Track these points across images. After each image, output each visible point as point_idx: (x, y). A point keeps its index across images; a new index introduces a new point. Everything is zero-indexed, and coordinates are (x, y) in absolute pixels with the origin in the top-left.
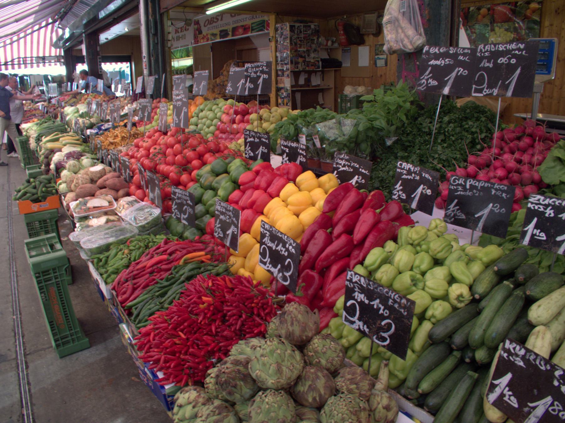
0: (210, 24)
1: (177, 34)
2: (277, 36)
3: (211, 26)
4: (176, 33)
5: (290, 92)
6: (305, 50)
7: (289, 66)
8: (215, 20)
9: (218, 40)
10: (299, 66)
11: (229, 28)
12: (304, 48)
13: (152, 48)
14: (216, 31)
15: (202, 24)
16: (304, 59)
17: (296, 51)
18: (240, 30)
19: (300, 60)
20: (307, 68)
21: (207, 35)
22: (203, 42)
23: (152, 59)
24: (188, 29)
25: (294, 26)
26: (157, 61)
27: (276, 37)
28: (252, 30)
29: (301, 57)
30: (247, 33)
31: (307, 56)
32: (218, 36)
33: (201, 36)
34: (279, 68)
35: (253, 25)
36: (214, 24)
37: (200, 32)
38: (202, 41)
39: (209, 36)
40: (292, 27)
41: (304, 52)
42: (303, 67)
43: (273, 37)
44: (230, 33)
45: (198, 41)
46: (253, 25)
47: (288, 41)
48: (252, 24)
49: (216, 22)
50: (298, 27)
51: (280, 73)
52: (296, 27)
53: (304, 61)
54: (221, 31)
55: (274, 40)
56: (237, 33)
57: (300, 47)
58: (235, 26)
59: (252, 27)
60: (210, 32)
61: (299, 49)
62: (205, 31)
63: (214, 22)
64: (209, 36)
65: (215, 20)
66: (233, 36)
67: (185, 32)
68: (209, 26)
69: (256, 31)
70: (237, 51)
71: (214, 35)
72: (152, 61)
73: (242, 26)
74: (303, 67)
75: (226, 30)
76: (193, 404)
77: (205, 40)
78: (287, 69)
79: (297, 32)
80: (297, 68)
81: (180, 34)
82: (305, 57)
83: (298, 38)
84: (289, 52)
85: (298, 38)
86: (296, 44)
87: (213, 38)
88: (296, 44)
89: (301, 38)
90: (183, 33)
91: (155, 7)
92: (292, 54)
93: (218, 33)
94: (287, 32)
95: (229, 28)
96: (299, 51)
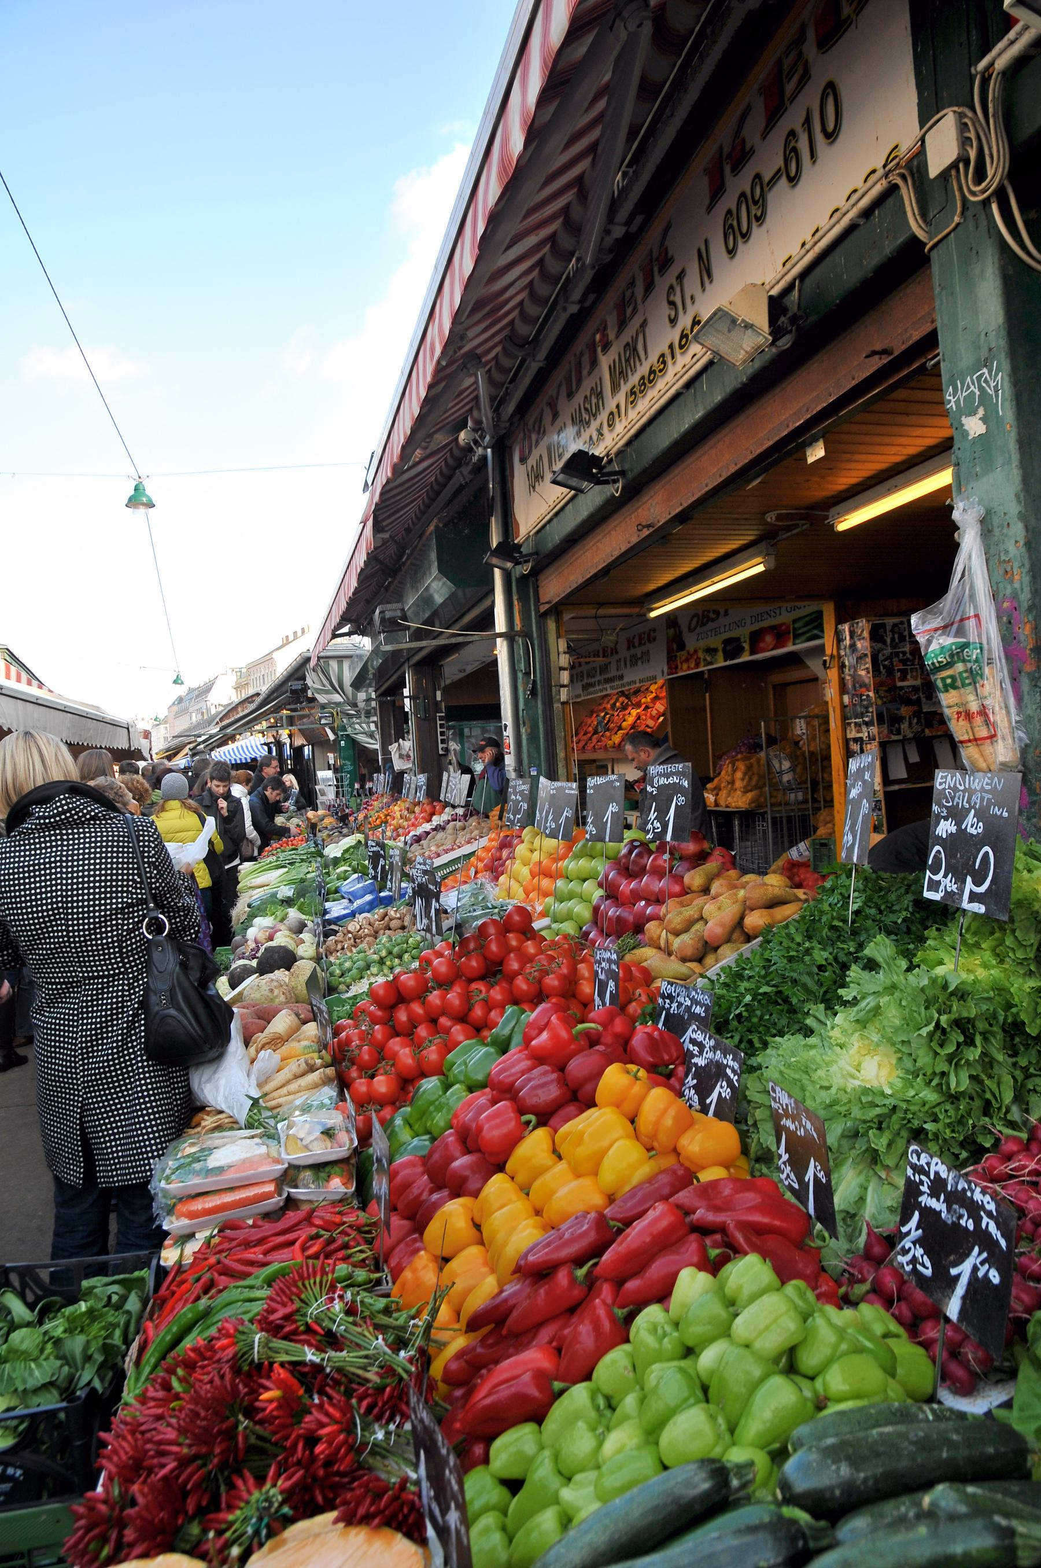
0: (703, 625)
1: (633, 651)
2: (842, 653)
3: (704, 628)
4: (629, 648)
5: (881, 796)
6: (918, 683)
7: (874, 730)
8: (712, 615)
9: (721, 663)
10: (904, 726)
11: (743, 633)
12: (915, 678)
13: (521, 706)
14: (716, 642)
15: (684, 628)
16: (916, 708)
17: (893, 688)
18: (769, 639)
19: (905, 711)
20: (927, 731)
21: (696, 651)
22: (689, 668)
23: (523, 730)
24: (655, 639)
25: (883, 625)
26: (533, 737)
27: (839, 657)
28: (796, 636)
29: (908, 702)
30: (784, 646)
31: (924, 700)
32: (720, 655)
33: (683, 654)
34: (852, 734)
35: (797, 625)
36: (711, 625)
37: (682, 646)
38: (685, 666)
39: (701, 655)
40: (876, 635)
41: (915, 689)
42: (917, 728)
43: (832, 656)
44: (746, 646)
45: (676, 667)
46: (797, 625)
47: (869, 665)
48: (794, 621)
49: (713, 620)
50: (895, 625)
51: (856, 747)
52: (888, 628)
53: (917, 714)
54: (726, 642)
55: (835, 663)
56: (762, 645)
57: (904, 678)
58: (756, 627)
59: (795, 629)
60: (703, 644)
61: (899, 684)
62: (692, 642)
63: (709, 619)
64: (701, 655)
65: (712, 615)
66: (752, 653)
67: (649, 646)
68: (699, 630)
69: (803, 638)
70: (774, 687)
71: (711, 651)
72: (524, 737)
73: (772, 628)
74: (917, 728)
75: (738, 639)
76: (197, 1166)
77: (692, 665)
78: (871, 738)
79: (893, 639)
80: (899, 733)
81: (638, 651)
82: (918, 702)
83: (897, 654)
84: (871, 694)
85: (897, 654)
86: (890, 671)
87: (709, 659)
88: (890, 671)
89: (904, 653)
90: (644, 648)
91: (529, 610)
92: (881, 698)
93: (720, 647)
94: (863, 645)
95: (743, 633)
96: (902, 688)
